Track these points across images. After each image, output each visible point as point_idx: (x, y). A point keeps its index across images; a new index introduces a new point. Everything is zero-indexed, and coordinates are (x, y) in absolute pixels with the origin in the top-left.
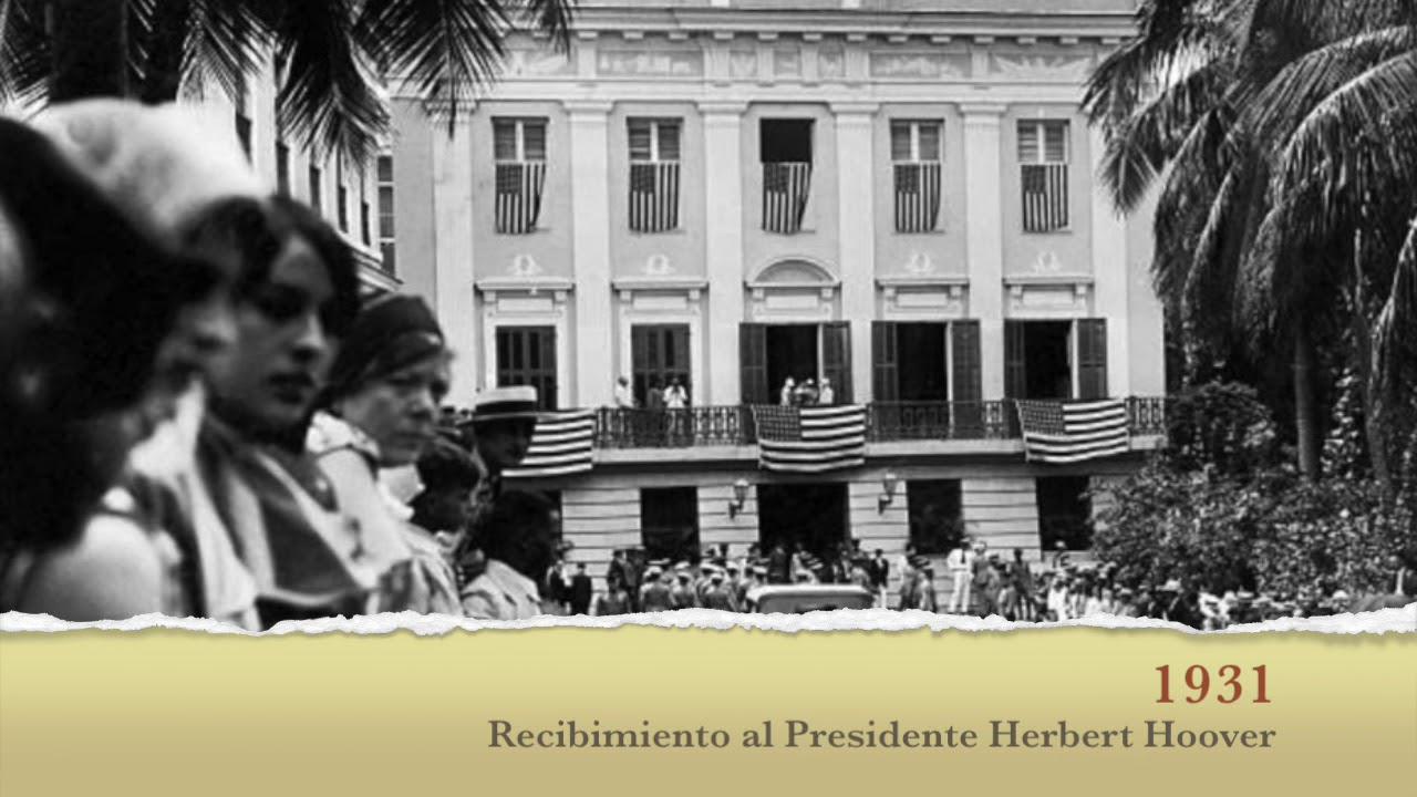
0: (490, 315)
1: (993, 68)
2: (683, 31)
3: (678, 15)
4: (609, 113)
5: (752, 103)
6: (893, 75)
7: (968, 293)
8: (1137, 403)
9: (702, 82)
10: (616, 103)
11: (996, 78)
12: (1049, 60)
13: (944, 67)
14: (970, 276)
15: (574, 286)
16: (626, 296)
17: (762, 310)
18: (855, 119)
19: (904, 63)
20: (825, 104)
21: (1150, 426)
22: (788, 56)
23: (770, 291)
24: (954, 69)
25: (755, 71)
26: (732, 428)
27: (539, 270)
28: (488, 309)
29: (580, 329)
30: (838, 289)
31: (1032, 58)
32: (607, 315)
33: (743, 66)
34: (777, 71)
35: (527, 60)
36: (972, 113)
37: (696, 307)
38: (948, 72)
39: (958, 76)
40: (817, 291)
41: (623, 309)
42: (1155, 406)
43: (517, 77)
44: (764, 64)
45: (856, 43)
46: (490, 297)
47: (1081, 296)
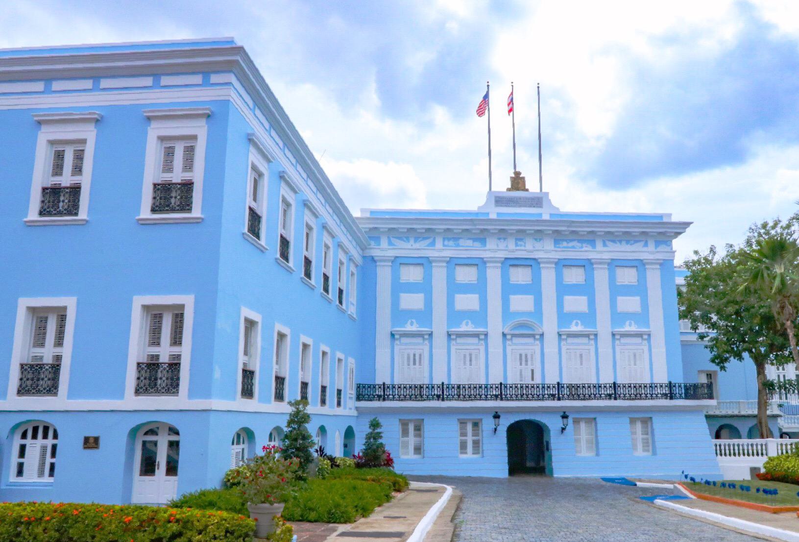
0: (453, 345)
1: (605, 245)
2: (478, 229)
3: (475, 222)
4: (448, 262)
5: (506, 259)
6: (564, 247)
7: (487, 337)
8: (503, 386)
9: (485, 250)
10: (451, 258)
11: (605, 249)
12: (628, 242)
13: (584, 245)
14: (433, 330)
15: (432, 332)
16: (618, 337)
17: (455, 344)
18: (441, 264)
19: (568, 243)
20: (535, 259)
21: (643, 395)
22: (521, 240)
23: (514, 336)
24: (588, 246)
25: (507, 246)
26: (363, 394)
27: (418, 326)
28: (397, 342)
29: (653, 350)
30: (542, 335)
31: (620, 241)
32: (557, 343)
33: (502, 245)
34: (517, 245)
35: (415, 242)
36: (597, 263)
37: (646, 342)
38: (586, 247)
39: (589, 248)
40: (533, 336)
41: (508, 342)
42: (680, 386)
43: (411, 248)
44: (511, 244)
45: (549, 234)
46: (509, 337)
47: (592, 339)
